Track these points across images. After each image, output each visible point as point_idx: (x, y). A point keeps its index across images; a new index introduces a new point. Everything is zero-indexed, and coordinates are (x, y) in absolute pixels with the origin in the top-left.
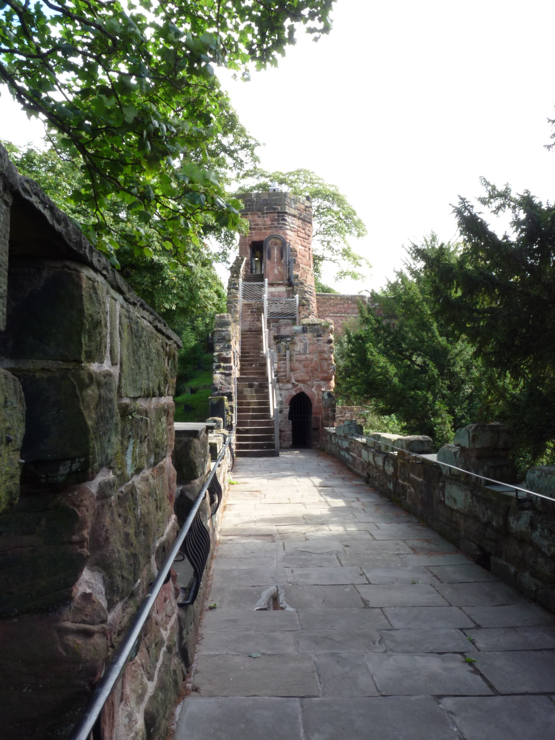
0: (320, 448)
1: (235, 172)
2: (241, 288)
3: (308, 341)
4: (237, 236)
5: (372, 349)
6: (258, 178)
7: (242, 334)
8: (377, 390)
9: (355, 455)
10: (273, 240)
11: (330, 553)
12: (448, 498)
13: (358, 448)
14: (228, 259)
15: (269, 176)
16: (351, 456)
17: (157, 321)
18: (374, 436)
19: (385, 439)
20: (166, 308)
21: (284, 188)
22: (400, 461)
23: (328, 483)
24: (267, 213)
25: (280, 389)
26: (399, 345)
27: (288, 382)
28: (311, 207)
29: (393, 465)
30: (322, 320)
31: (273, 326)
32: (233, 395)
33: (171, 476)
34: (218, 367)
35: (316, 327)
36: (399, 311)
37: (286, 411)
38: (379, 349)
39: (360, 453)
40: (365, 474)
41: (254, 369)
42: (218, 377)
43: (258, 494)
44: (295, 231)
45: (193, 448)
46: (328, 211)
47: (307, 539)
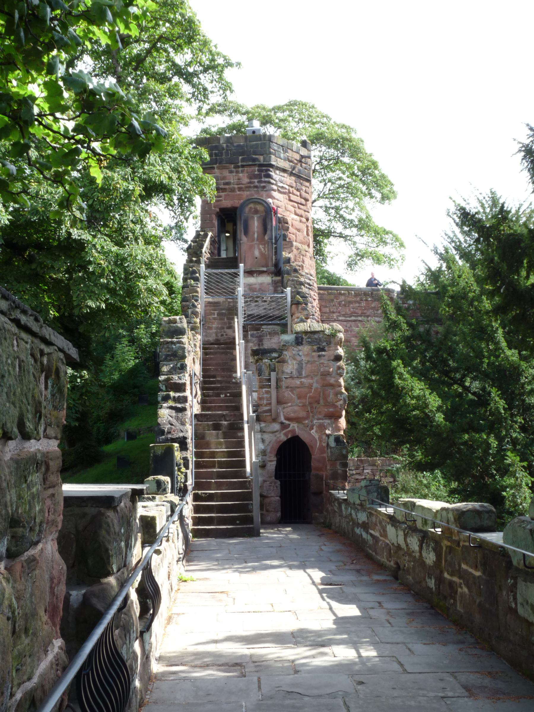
0: (324, 523)
1: (196, 105)
2: (202, 278)
3: (303, 358)
4: (198, 200)
5: (401, 369)
6: (230, 115)
7: (204, 348)
8: (411, 431)
9: (377, 534)
10: (252, 205)
11: (332, 696)
12: (522, 604)
13: (380, 523)
14: (185, 236)
15: (247, 113)
16: (371, 535)
17: (18, 311)
18: (405, 504)
19: (423, 508)
20: (90, 307)
21: (270, 130)
22: (446, 543)
23: (335, 579)
24: (243, 166)
25: (262, 431)
26: (445, 362)
27: (274, 420)
28: (309, 157)
29: (435, 550)
30: (326, 326)
31: (252, 336)
32: (189, 441)
33: (55, 573)
34: (166, 398)
35: (316, 336)
36: (444, 310)
37: (272, 466)
38: (414, 368)
39: (385, 531)
40: (392, 563)
41: (223, 401)
42: (165, 414)
43: (223, 596)
44: (284, 193)
45: (105, 526)
46: (336, 163)
47: (296, 672)
